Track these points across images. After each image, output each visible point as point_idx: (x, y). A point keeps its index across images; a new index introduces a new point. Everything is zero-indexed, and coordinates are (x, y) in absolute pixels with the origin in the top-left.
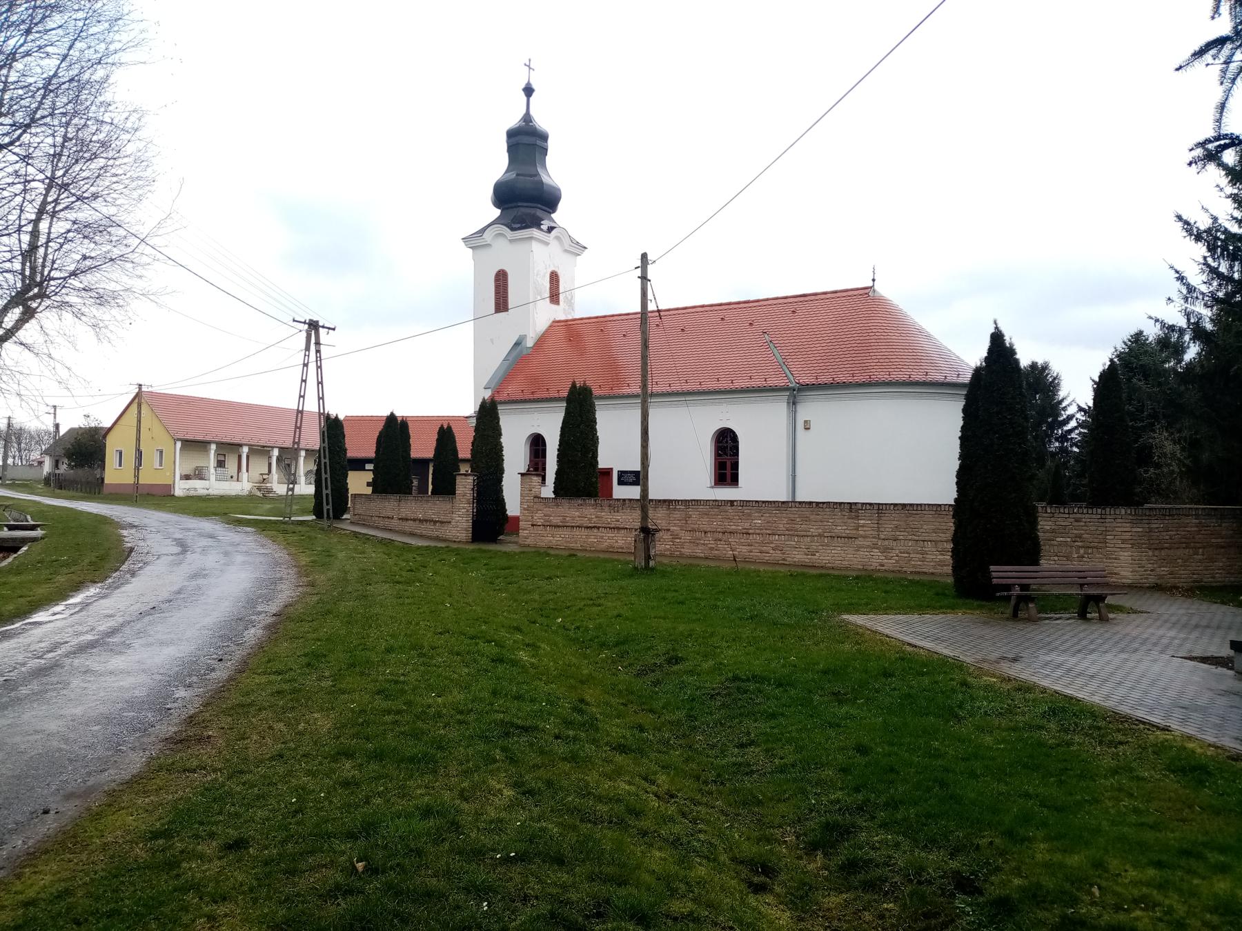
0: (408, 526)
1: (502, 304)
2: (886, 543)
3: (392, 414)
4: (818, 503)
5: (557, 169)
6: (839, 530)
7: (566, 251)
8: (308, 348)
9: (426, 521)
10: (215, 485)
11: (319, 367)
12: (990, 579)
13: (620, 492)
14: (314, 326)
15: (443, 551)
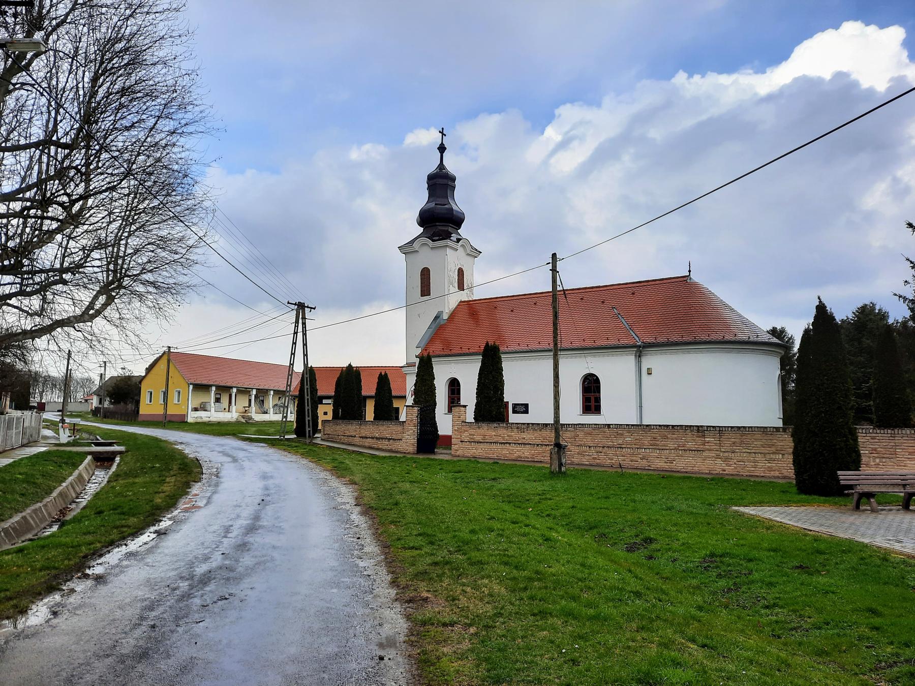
0: (368, 442)
1: (425, 290)
2: (726, 454)
3: (350, 365)
4: (673, 426)
5: (461, 200)
6: (690, 445)
7: (468, 254)
8: (297, 322)
9: (382, 439)
10: (215, 415)
11: (304, 334)
12: (838, 481)
13: (513, 418)
14: (301, 306)
15: (397, 458)
